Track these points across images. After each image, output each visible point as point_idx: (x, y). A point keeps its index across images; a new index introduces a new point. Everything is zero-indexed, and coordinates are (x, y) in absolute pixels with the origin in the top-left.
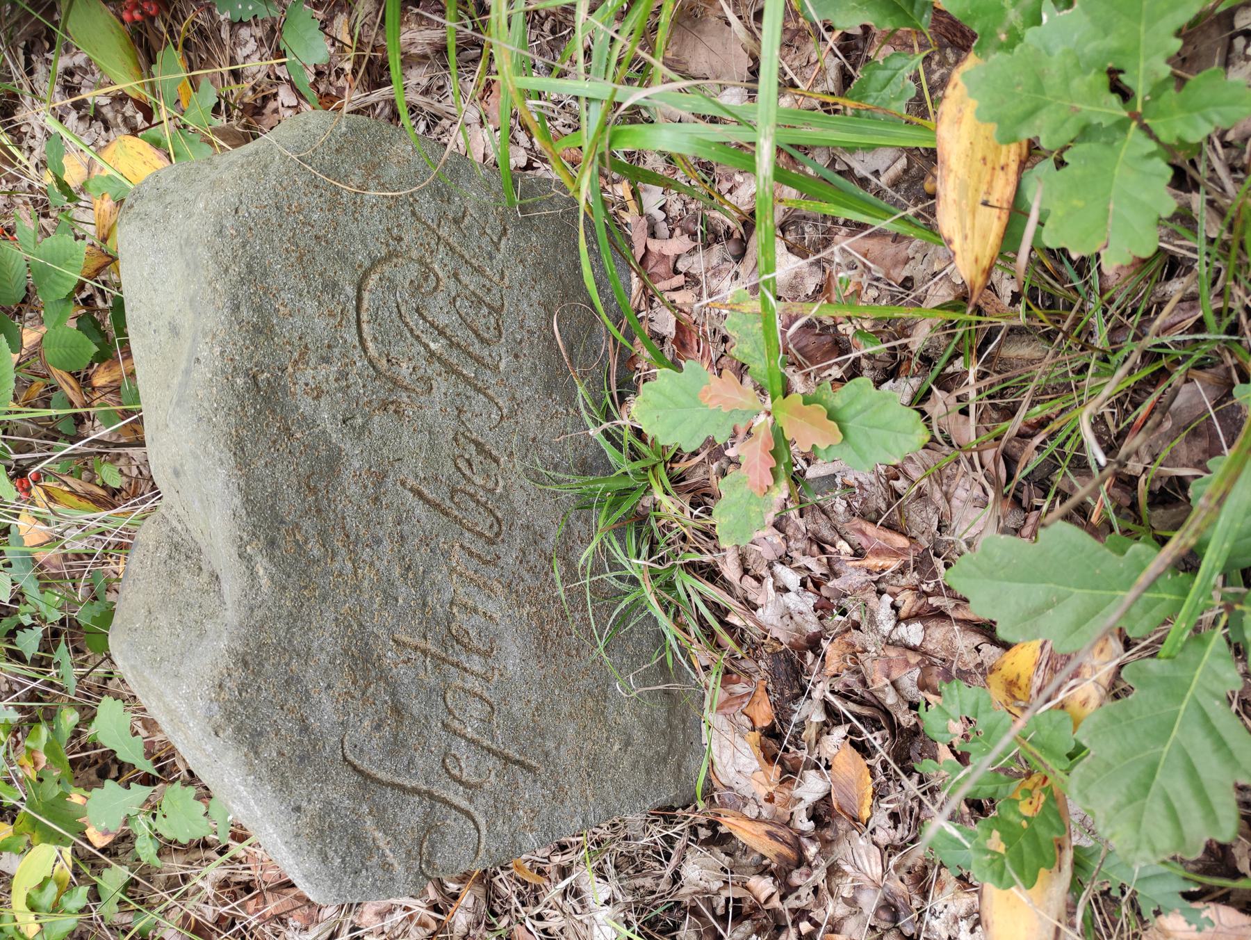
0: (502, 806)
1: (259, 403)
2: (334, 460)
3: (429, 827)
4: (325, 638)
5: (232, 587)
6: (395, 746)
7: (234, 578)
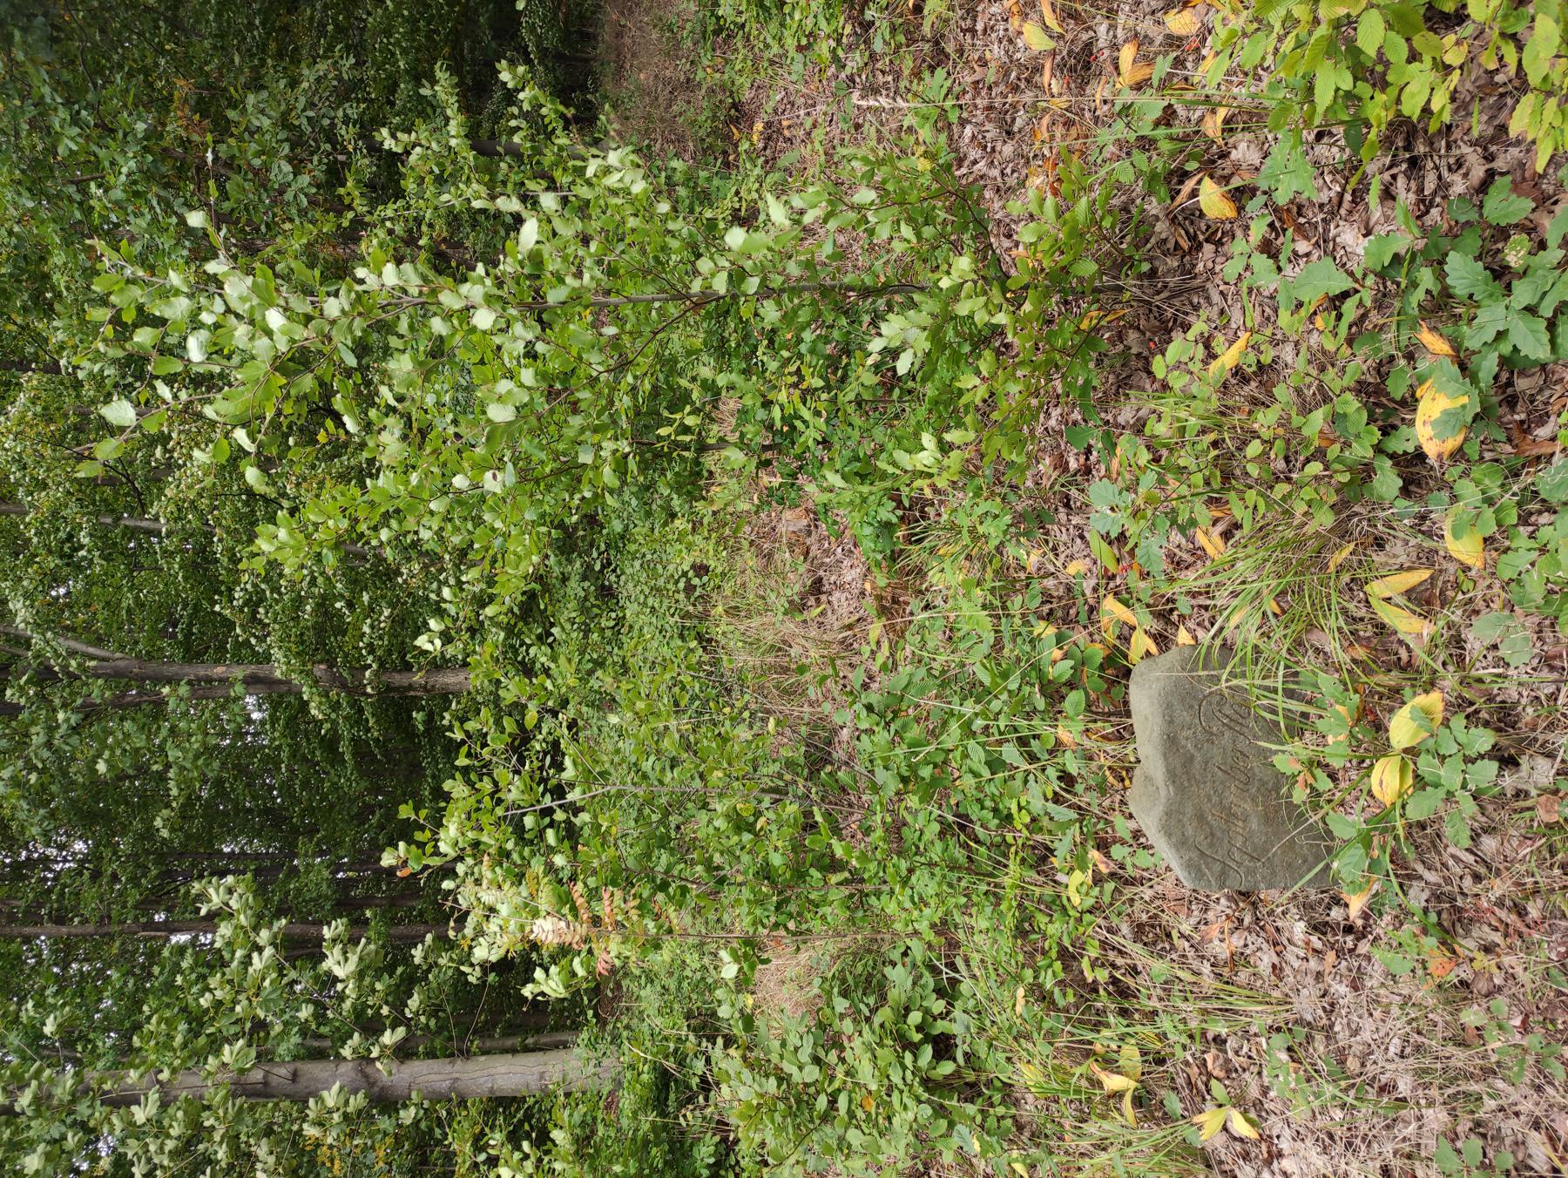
0: (1250, 872)
1: (1171, 742)
2: (1192, 757)
3: (1223, 873)
4: (1189, 810)
5: (1163, 792)
6: (1211, 845)
7: (1164, 791)
